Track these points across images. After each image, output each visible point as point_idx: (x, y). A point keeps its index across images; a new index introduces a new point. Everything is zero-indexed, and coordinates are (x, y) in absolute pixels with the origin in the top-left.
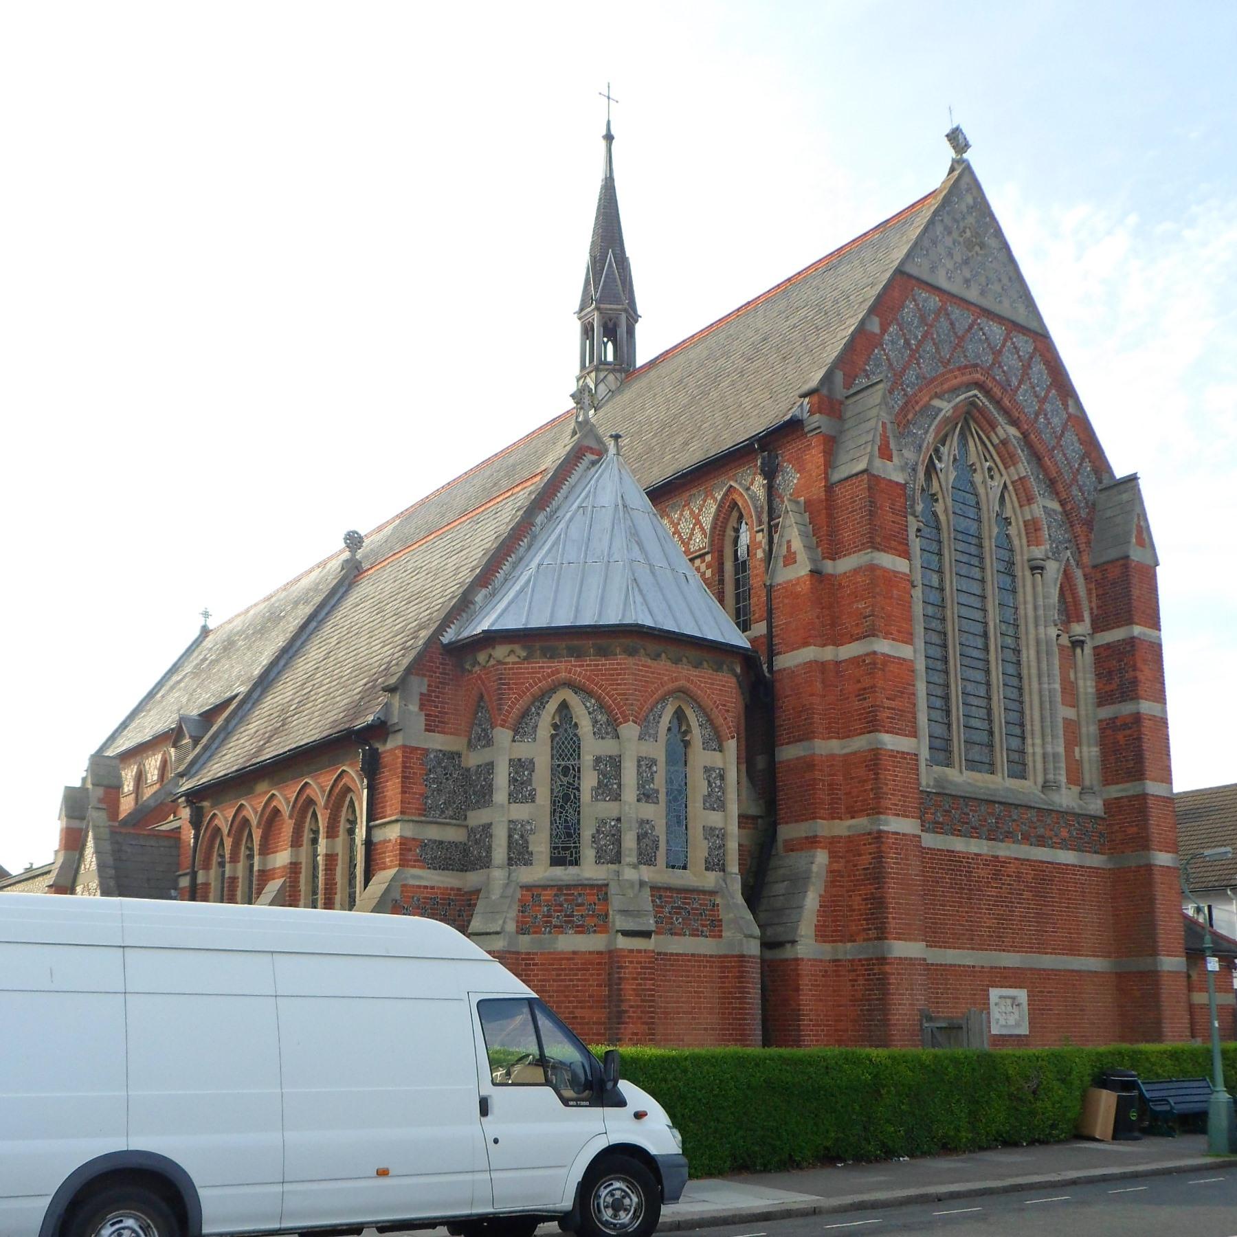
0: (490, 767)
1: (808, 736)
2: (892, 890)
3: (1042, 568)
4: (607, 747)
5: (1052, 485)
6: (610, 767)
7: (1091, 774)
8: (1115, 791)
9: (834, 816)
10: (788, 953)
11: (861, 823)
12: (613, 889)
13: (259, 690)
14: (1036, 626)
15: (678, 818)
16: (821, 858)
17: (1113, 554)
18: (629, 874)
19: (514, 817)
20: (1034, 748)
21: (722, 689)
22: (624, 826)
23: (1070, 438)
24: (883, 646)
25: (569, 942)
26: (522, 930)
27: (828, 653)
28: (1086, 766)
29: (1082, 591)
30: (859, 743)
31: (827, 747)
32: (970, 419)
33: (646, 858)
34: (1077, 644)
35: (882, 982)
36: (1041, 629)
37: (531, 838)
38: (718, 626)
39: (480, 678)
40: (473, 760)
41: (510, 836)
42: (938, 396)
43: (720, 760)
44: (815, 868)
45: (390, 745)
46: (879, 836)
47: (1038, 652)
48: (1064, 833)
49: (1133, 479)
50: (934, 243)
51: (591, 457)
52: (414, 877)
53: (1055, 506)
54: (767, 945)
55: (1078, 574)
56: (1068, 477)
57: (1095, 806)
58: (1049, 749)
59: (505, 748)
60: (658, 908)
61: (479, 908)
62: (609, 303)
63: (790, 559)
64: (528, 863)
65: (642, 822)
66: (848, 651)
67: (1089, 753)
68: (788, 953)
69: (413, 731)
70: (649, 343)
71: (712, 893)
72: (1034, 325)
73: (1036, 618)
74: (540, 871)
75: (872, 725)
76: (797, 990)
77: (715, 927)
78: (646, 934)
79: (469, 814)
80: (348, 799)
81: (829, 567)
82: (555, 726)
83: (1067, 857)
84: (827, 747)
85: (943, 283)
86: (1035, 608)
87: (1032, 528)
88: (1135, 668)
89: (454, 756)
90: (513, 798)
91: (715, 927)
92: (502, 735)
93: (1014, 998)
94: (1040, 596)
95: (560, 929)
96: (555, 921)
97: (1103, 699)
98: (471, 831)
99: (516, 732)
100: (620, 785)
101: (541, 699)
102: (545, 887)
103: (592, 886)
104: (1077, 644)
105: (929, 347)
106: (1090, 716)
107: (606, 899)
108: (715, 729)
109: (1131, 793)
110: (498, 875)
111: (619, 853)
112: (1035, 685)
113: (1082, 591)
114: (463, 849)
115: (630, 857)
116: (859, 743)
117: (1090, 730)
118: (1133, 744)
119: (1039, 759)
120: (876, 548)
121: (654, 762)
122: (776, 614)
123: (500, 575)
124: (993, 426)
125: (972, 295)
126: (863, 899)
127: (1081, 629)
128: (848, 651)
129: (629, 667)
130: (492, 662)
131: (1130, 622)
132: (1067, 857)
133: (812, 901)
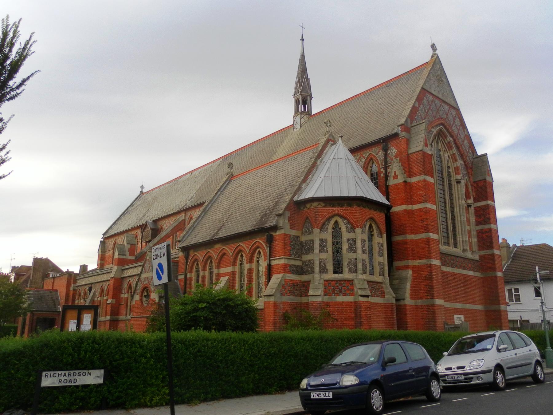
0: (312, 241)
1: (404, 233)
2: (435, 282)
3: (460, 182)
4: (351, 235)
5: (462, 156)
6: (353, 243)
7: (475, 248)
8: (483, 253)
9: (414, 259)
10: (402, 303)
11: (424, 261)
12: (356, 281)
13: (203, 214)
14: (459, 200)
15: (371, 259)
16: (410, 272)
17: (480, 178)
18: (361, 277)
19: (321, 257)
20: (459, 238)
21: (380, 217)
22: (358, 261)
23: (466, 141)
24: (429, 206)
25: (341, 299)
26: (325, 295)
27: (410, 207)
28: (473, 244)
29: (470, 190)
30: (422, 236)
31: (411, 237)
32: (440, 135)
33: (364, 272)
34: (469, 206)
35: (434, 312)
36: (460, 201)
37: (327, 265)
38: (378, 196)
39: (307, 212)
40: (303, 239)
41: (320, 264)
42: (433, 127)
43: (380, 241)
44: (409, 275)
45: (278, 233)
46: (431, 266)
47: (460, 208)
48: (470, 266)
49: (486, 155)
50: (430, 79)
51: (331, 143)
52: (288, 277)
53: (462, 162)
54: (397, 300)
55: (469, 184)
56: (466, 154)
57: (477, 257)
58: (464, 239)
59: (316, 236)
60: (372, 289)
61: (311, 286)
62: (303, 98)
63: (395, 177)
64: (326, 273)
65: (363, 260)
66: (416, 207)
67: (474, 240)
68: (402, 303)
69: (285, 229)
70: (317, 106)
71: (381, 283)
72: (455, 106)
73: (459, 198)
74: (330, 276)
75: (427, 230)
76: (406, 315)
77: (382, 294)
78: (368, 296)
79: (303, 256)
80: (257, 251)
81: (409, 180)
82: (333, 229)
83: (471, 273)
84: (411, 237)
85: (433, 92)
86: (458, 195)
87: (457, 169)
88: (489, 214)
89: (298, 237)
90: (320, 251)
91: (382, 294)
92: (316, 231)
93: (460, 318)
94: (459, 191)
95: (337, 294)
96: (336, 292)
97: (478, 224)
98: (304, 262)
99: (321, 230)
100: (356, 248)
101: (329, 219)
102: (332, 281)
103: (348, 281)
104: (469, 206)
105: (430, 112)
106: (474, 229)
107: (353, 285)
108: (380, 231)
109: (489, 253)
110: (317, 276)
111: (356, 270)
112: (459, 219)
113: (470, 190)
114: (301, 268)
115: (360, 271)
116: (422, 236)
117: (474, 233)
118: (487, 237)
119: (461, 241)
120: (426, 174)
121: (365, 241)
122: (390, 194)
123: (309, 179)
124: (446, 137)
125: (440, 96)
126: (425, 284)
127: (470, 201)
128: (416, 207)
129: (356, 211)
130: (312, 207)
131: (487, 199)
132: (471, 273)
133: (408, 286)
